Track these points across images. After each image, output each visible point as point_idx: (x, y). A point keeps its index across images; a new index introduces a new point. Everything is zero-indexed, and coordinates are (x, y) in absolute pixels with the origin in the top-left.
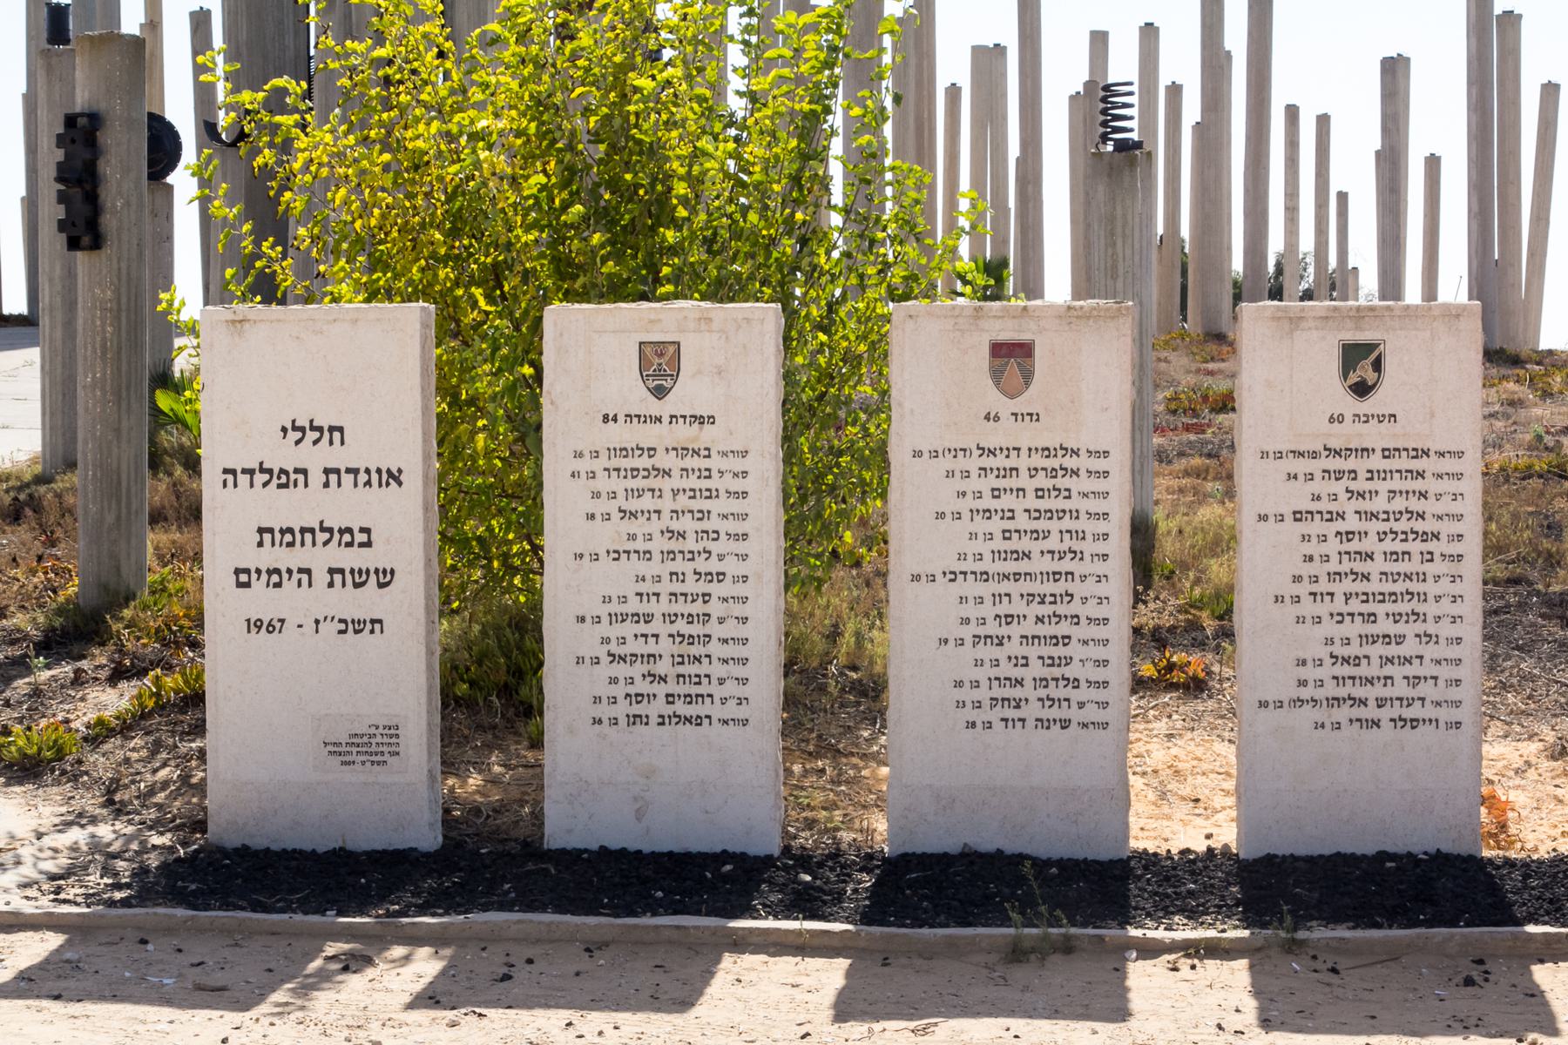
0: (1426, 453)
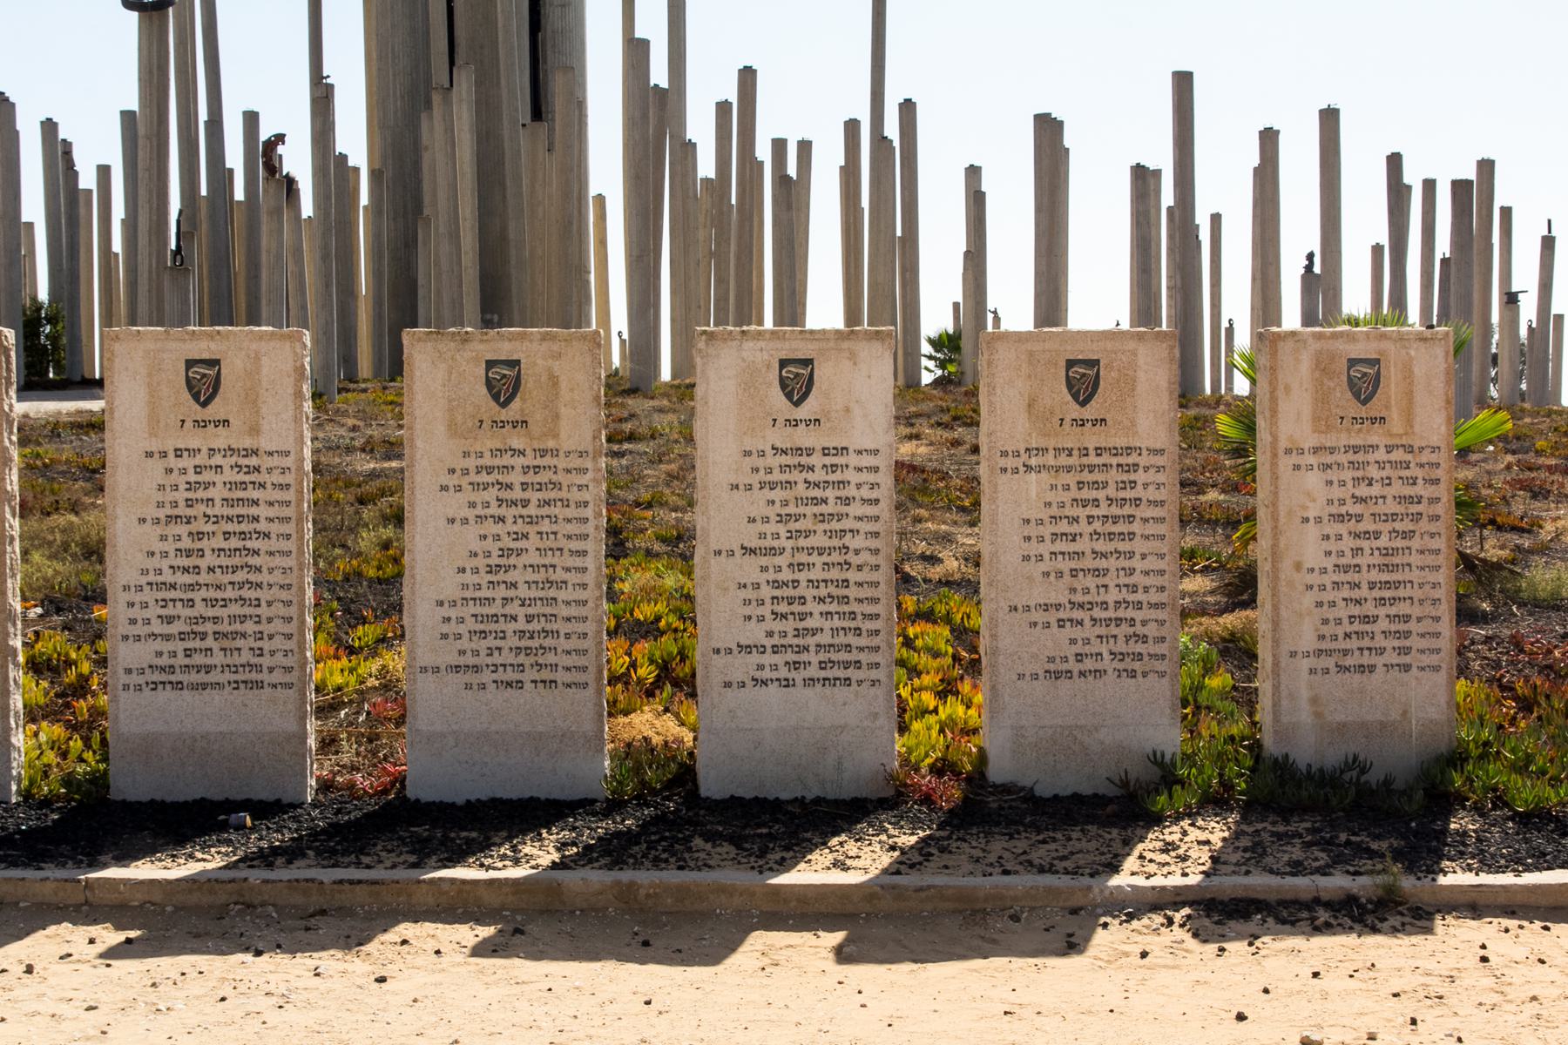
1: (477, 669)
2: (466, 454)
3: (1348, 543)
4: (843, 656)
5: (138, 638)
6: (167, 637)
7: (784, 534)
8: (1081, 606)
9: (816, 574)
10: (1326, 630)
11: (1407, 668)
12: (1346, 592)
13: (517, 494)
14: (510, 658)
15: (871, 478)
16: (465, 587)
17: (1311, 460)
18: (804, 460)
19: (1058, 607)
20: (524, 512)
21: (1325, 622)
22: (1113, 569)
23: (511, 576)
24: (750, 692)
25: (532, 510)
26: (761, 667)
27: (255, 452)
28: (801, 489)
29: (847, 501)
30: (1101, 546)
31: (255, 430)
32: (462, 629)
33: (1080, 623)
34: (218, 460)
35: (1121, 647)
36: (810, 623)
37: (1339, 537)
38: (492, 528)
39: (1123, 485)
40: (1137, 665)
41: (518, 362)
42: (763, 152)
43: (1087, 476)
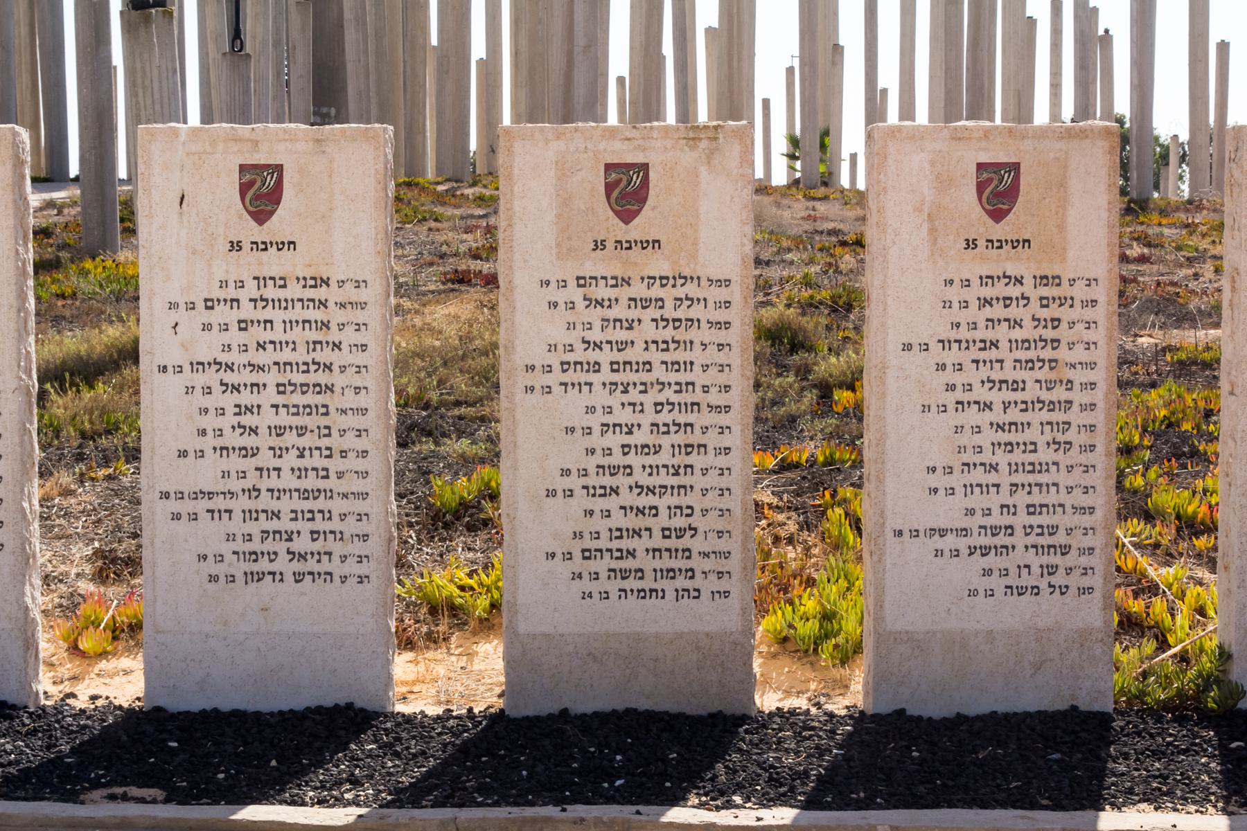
0: (326, 282)
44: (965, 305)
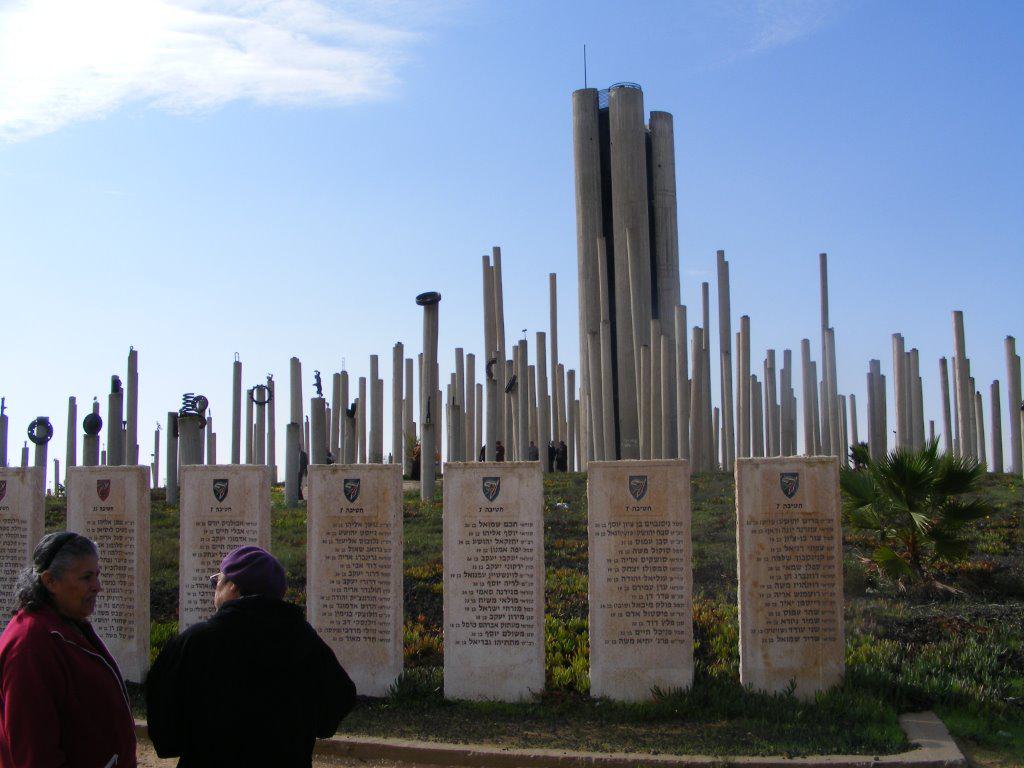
1: (339, 631)
2: (335, 525)
3: (782, 572)
4: (514, 629)
5: (192, 610)
6: (204, 610)
7: (485, 566)
8: (639, 605)
9: (502, 587)
10: (772, 619)
11: (817, 639)
12: (782, 598)
13: (358, 545)
14: (354, 626)
15: (529, 538)
16: (334, 590)
17: (762, 527)
18: (495, 529)
19: (626, 605)
20: (361, 554)
21: (771, 614)
22: (655, 586)
23: (355, 585)
24: (469, 646)
25: (364, 553)
26: (474, 634)
27: (242, 523)
28: (494, 543)
29: (517, 550)
30: (649, 573)
31: (242, 513)
32: (333, 611)
33: (638, 614)
34: (226, 527)
35: (660, 627)
36: (498, 612)
37: (778, 569)
38: (346, 561)
39: (661, 542)
40: (669, 637)
41: (359, 480)
42: (757, 369)
43: (641, 537)
44: (93, 530)
